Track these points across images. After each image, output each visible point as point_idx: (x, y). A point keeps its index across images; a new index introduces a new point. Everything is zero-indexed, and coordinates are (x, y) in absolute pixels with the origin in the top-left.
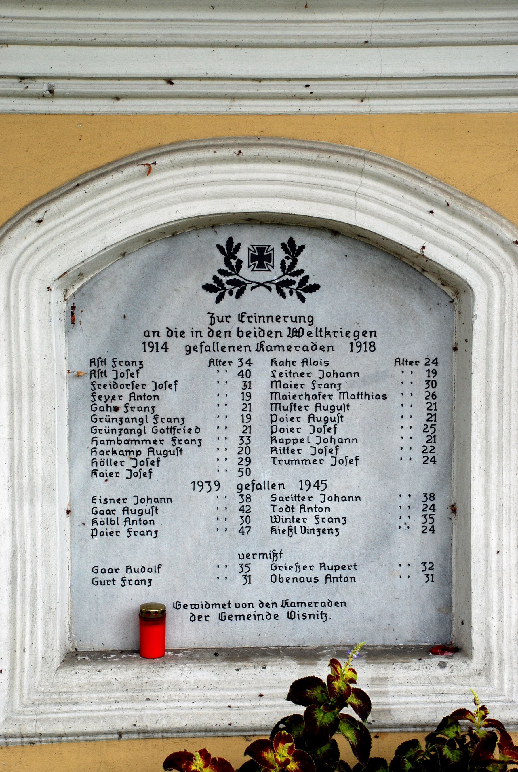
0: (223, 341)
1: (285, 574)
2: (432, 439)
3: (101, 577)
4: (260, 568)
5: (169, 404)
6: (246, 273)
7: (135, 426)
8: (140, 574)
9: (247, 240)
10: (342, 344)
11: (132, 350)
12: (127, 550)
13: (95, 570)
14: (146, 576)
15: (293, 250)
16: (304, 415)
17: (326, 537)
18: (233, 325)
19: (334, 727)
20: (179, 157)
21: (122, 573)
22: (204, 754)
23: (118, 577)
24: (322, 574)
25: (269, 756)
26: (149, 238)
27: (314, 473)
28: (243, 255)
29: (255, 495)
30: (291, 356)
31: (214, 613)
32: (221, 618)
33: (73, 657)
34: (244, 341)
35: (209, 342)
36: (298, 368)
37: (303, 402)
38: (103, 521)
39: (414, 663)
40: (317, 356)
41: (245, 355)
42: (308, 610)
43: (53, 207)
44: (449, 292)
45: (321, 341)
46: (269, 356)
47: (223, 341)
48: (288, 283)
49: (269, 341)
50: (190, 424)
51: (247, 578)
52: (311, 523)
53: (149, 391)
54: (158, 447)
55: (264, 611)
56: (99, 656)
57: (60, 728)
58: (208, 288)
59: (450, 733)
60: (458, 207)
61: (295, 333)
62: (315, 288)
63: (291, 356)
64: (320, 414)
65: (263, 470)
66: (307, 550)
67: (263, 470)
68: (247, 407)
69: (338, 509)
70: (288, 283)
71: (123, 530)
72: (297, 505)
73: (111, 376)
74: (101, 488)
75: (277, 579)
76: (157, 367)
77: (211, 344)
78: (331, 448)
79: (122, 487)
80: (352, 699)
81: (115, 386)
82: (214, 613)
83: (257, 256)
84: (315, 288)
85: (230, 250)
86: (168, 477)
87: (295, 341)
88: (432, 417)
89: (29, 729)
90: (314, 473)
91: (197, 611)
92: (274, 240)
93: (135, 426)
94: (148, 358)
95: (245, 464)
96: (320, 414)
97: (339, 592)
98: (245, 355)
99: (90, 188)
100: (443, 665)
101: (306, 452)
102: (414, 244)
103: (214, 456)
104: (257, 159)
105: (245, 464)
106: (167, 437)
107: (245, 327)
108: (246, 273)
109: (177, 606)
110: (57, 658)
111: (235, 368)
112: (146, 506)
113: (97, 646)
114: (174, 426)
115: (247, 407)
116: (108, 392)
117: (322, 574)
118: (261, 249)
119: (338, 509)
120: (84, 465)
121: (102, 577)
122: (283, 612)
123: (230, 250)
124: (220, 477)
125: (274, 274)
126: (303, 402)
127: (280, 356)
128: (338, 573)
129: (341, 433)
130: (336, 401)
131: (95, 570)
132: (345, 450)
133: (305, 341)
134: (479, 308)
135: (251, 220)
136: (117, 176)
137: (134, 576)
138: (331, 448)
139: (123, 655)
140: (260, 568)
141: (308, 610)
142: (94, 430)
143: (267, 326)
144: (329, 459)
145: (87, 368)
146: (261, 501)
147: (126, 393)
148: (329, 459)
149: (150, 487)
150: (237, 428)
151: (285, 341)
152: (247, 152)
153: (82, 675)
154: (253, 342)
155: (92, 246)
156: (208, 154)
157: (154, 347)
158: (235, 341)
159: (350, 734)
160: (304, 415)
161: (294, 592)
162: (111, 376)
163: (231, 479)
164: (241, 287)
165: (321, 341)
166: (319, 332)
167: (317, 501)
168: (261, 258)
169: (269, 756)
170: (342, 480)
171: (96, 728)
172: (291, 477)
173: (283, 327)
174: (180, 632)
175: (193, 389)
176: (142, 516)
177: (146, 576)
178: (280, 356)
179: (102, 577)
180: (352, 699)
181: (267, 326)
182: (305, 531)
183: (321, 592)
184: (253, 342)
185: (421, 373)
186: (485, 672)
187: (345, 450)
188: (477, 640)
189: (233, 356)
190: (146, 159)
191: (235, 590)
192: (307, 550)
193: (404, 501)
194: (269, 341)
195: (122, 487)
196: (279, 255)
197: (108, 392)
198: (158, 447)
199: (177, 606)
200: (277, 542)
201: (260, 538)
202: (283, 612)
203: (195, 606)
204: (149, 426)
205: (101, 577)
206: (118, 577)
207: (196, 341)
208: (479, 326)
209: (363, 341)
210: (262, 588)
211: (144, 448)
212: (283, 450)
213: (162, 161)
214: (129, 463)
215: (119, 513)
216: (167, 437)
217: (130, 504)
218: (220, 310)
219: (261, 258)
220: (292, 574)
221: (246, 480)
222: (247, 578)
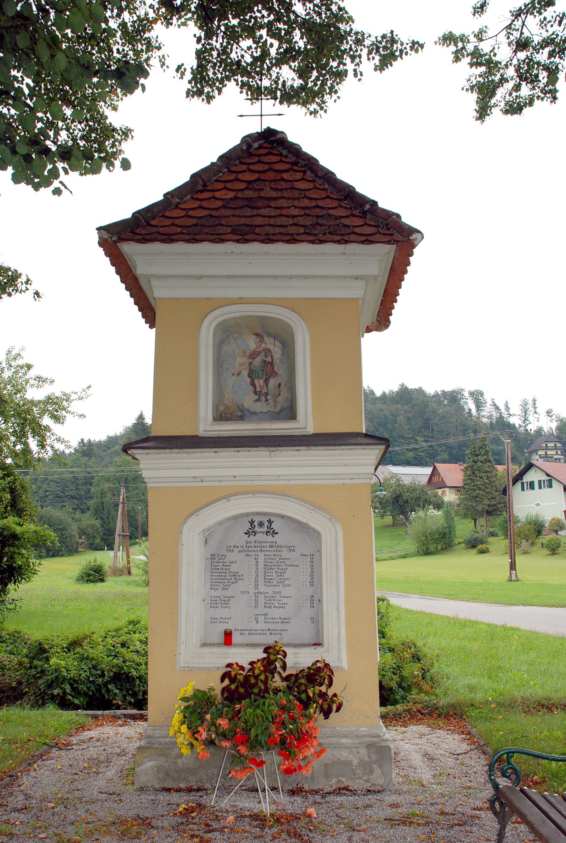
0: (250, 549)
1: (269, 621)
2: (312, 579)
3: (213, 620)
4: (261, 618)
5: (234, 568)
6: (257, 529)
7: (224, 574)
8: (224, 620)
9: (257, 519)
10: (285, 550)
11: (223, 552)
12: (221, 612)
13: (211, 618)
14: (226, 620)
15: (270, 522)
16: (274, 571)
17: (281, 609)
18: (253, 544)
19: (275, 660)
20: (237, 497)
21: (219, 619)
22: (237, 663)
23: (218, 621)
24: (280, 621)
25: (255, 665)
26: (228, 519)
27: (277, 589)
28: (256, 524)
29: (259, 595)
30: (270, 553)
31: (247, 632)
32: (249, 634)
33: (204, 645)
34: (256, 549)
35: (246, 549)
36: (272, 557)
37: (274, 567)
38: (214, 603)
39: (307, 648)
40: (278, 553)
41: (256, 553)
42: (276, 632)
43: (201, 511)
44: (315, 535)
45: (279, 549)
46: (264, 553)
47: (250, 549)
48: (269, 532)
49: (263, 549)
50: (240, 574)
51: (257, 622)
52: (276, 605)
53: (228, 564)
54: (230, 581)
55: (262, 632)
56: (212, 645)
57: (200, 666)
58: (246, 533)
59: (314, 667)
60: (316, 510)
61: (271, 546)
62: (277, 533)
63: (270, 553)
64: (279, 571)
65: (262, 588)
66: (276, 613)
67: (262, 588)
68: (257, 569)
69: (285, 600)
70: (269, 532)
71: (220, 606)
72: (272, 599)
73: (217, 559)
74: (383, 709)
75: (266, 622)
76: (230, 557)
77: (246, 550)
78: (282, 581)
79: (219, 593)
80: (281, 652)
81: (218, 562)
82: (247, 632)
83: (260, 526)
84: (277, 533)
85: (252, 522)
86: (232, 590)
87: (271, 549)
88: (312, 572)
89: (191, 665)
90: (277, 589)
91: (242, 632)
92: (265, 519)
93: (224, 574)
94: (228, 554)
95: (256, 586)
96: (279, 571)
97: (285, 626)
98: (256, 553)
99: (211, 506)
100: (315, 649)
101: (275, 582)
102: (304, 521)
103: (247, 584)
104: (259, 497)
105: (256, 586)
106: (233, 578)
107: (256, 545)
108: (257, 529)
109: (236, 630)
110: (199, 644)
111: (253, 557)
112: (226, 599)
113: (212, 642)
114: (235, 574)
115: (257, 569)
116: (216, 564)
117: (280, 621)
118: (261, 522)
119: (285, 600)
120: (208, 586)
121: (213, 620)
122: (268, 633)
123: (252, 522)
124: (249, 590)
125: (265, 529)
126: (274, 567)
127: (267, 553)
128: (285, 621)
129: (285, 577)
130: (284, 567)
131: (211, 618)
132: (287, 582)
133: (274, 549)
134: (323, 539)
135: (258, 514)
136: (219, 502)
137: (223, 621)
138: (282, 581)
139: (219, 645)
140: (261, 618)
141: (276, 632)
142: (211, 575)
143: (263, 545)
144: (282, 585)
145: (210, 557)
146: (261, 598)
147: (221, 564)
148: (282, 585)
149: (228, 593)
150: (254, 575)
151: (268, 549)
152: (256, 495)
153: (206, 650)
154: (259, 549)
155: (211, 522)
156: (245, 496)
157: (230, 551)
158: (253, 549)
159: (281, 663)
160: (274, 571)
161: (271, 626)
162: (217, 559)
163: (252, 591)
164: (255, 533)
165: (279, 549)
166: (278, 546)
167: (278, 598)
168: (261, 524)
169: (255, 665)
170: (286, 591)
171: (211, 666)
172: (270, 590)
173: (267, 544)
174: (236, 638)
175: (241, 563)
176: (225, 602)
177: (226, 620)
178: (267, 553)
179: (213, 620)
180: (281, 652)
181: (263, 545)
182: (275, 607)
183: (280, 626)
184: (259, 549)
185: (309, 558)
186: (327, 651)
187: (287, 582)
188: (325, 641)
189: (253, 553)
190: (227, 497)
191: (253, 625)
192: (276, 613)
193: (305, 598)
194: (263, 549)
195: (219, 593)
196: (266, 524)
197: (216, 564)
198: (230, 581)
199: (236, 630)
200: (267, 610)
201: (261, 609)
202: (268, 633)
203: (241, 630)
204: (228, 574)
205: (213, 620)
206: (218, 621)
207: (242, 549)
208: (323, 545)
209: (291, 549)
210: (262, 625)
211: (226, 581)
212: (268, 582)
213: (233, 498)
214: (222, 586)
215: (219, 601)
216: (233, 578)
217: (222, 598)
218: (249, 540)
219: (261, 524)
220: (271, 621)
221: (257, 591)
222: (257, 622)
